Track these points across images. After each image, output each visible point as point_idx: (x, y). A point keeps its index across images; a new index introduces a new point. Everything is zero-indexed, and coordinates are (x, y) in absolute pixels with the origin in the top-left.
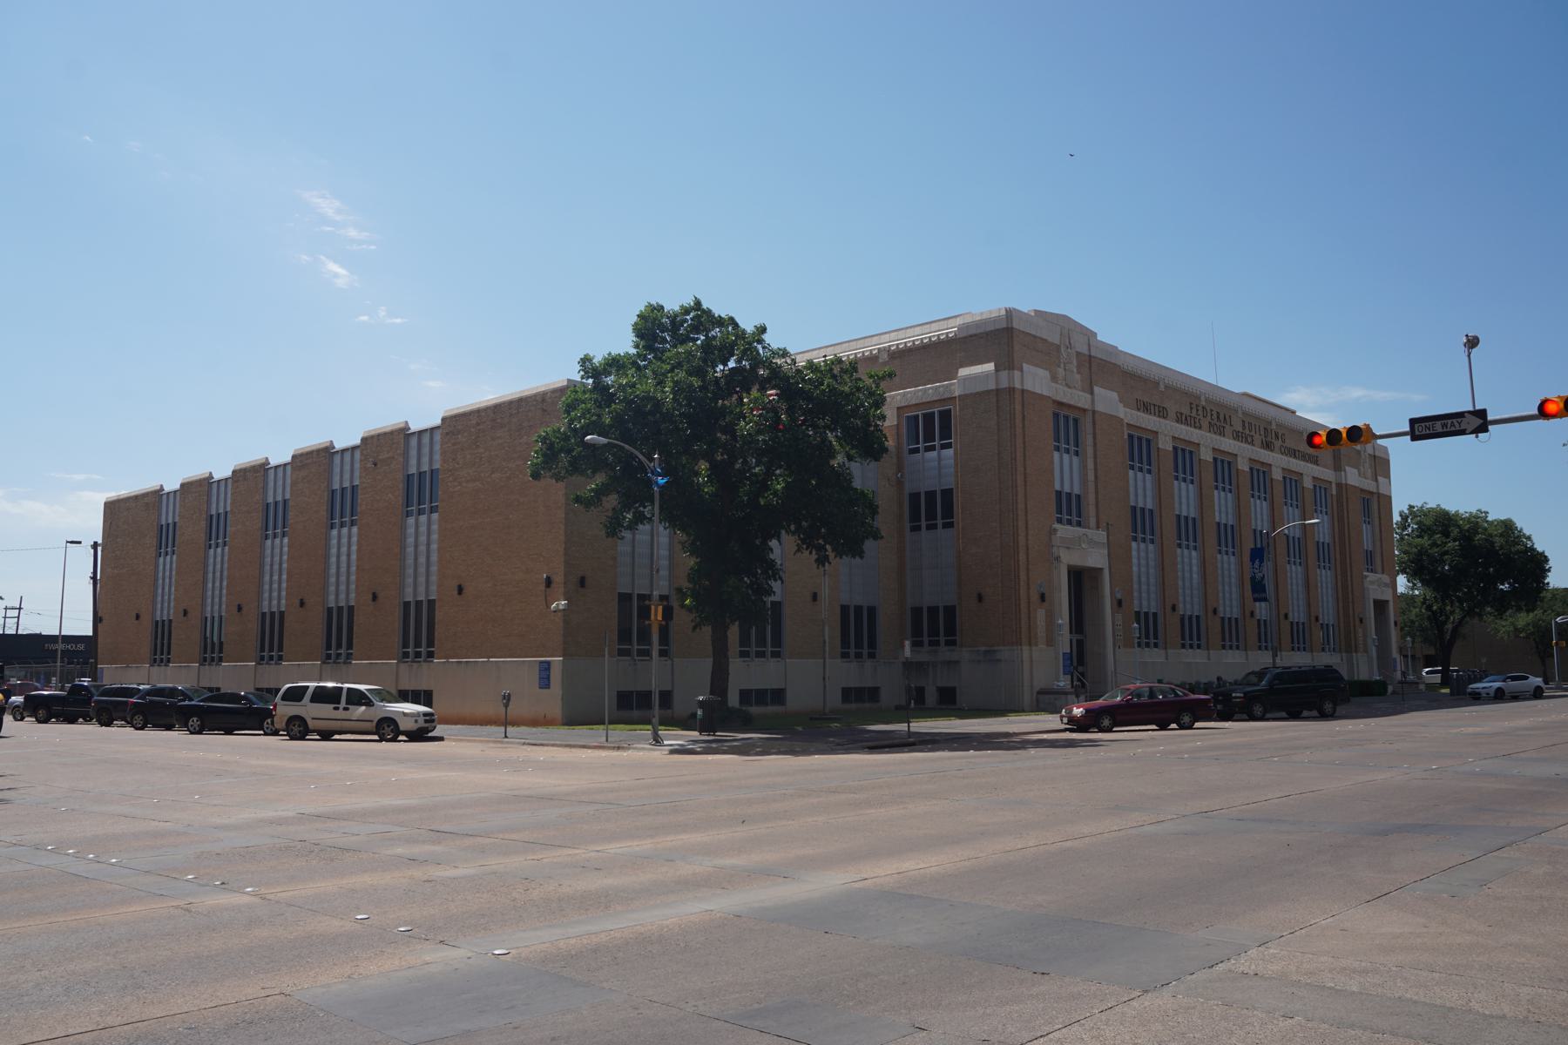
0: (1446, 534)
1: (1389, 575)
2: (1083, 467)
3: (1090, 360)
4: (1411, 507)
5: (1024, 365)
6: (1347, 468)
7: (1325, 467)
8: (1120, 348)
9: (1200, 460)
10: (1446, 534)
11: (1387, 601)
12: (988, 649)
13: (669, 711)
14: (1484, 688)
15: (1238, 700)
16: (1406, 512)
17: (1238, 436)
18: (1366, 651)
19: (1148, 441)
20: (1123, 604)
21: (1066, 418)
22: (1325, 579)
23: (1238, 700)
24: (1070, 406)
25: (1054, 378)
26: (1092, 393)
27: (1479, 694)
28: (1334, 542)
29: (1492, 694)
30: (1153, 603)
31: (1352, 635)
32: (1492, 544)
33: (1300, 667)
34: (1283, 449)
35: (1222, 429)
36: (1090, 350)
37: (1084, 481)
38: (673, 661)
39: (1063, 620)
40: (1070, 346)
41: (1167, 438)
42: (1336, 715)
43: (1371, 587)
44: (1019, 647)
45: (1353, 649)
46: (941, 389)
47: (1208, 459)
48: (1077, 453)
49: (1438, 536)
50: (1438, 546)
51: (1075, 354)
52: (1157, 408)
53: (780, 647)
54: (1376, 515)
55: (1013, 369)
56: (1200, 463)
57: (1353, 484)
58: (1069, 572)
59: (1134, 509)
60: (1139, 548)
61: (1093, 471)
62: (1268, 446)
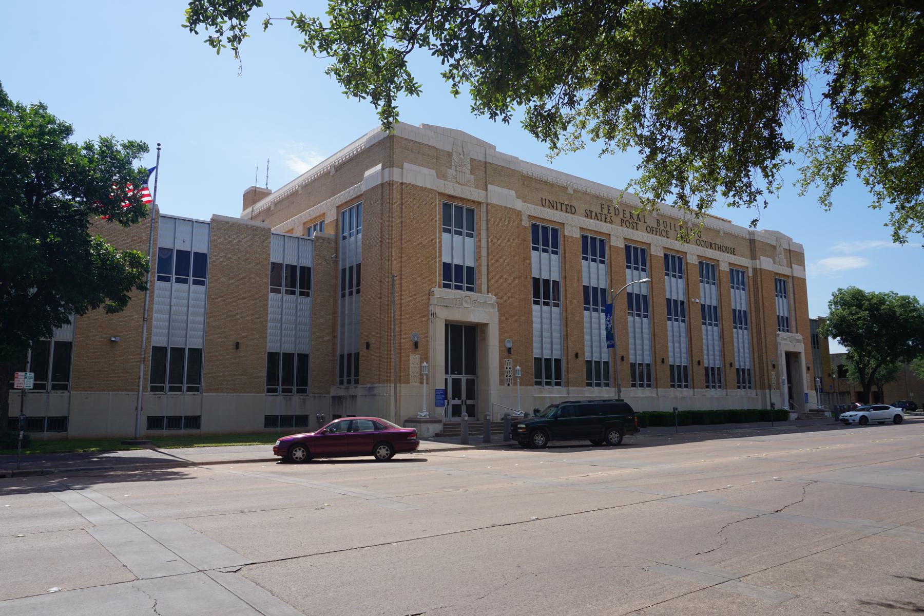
0: (860, 306)
1: (802, 335)
2: (478, 246)
3: (485, 167)
4: (840, 290)
5: (405, 164)
6: (761, 257)
7: (742, 256)
8: (794, 241)
9: (610, 246)
10: (860, 306)
11: (800, 353)
12: (371, 386)
13: (65, 433)
14: (851, 416)
15: (521, 430)
16: (837, 293)
17: (651, 230)
18: (778, 388)
19: (680, 259)
20: (420, 344)
21: (738, 271)
22: (741, 338)
23: (521, 430)
24: (462, 199)
25: (774, 263)
26: (791, 268)
27: (847, 420)
28: (751, 310)
29: (857, 421)
30: (747, 364)
31: (766, 377)
32: (894, 312)
33: (604, 401)
34: (699, 243)
35: (635, 225)
36: (486, 158)
37: (478, 256)
38: (70, 393)
39: (785, 377)
40: (780, 246)
41: (574, 228)
42: (622, 443)
43: (782, 342)
44: (389, 384)
45: (767, 386)
46: (352, 192)
47: (659, 254)
48: (785, 297)
49: (855, 308)
50: (853, 315)
51: (469, 160)
52: (717, 246)
53: (199, 384)
54: (791, 291)
55: (393, 167)
56: (610, 248)
57: (767, 268)
58: (446, 326)
59: (734, 310)
60: (707, 330)
61: (486, 249)
62: (685, 238)
